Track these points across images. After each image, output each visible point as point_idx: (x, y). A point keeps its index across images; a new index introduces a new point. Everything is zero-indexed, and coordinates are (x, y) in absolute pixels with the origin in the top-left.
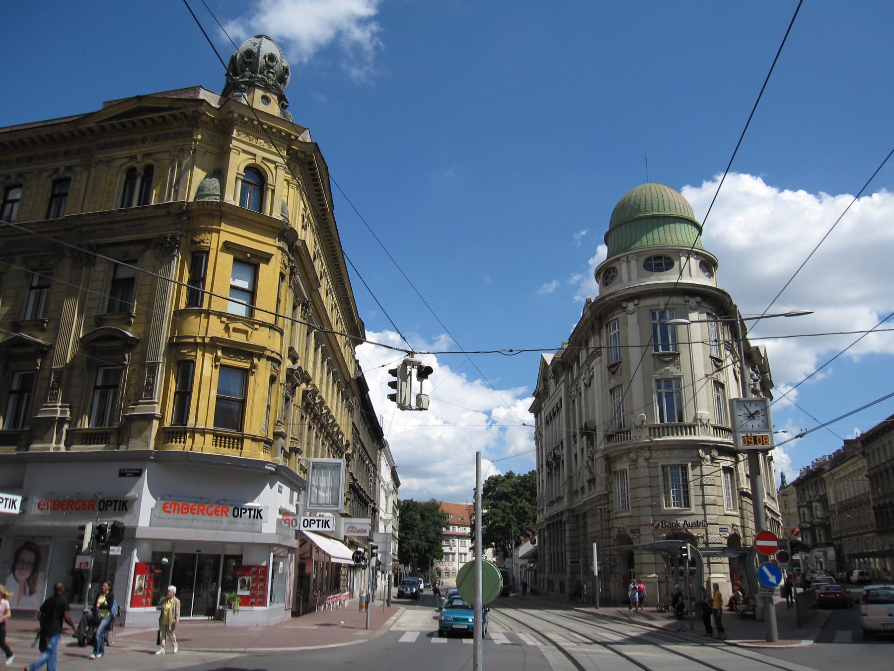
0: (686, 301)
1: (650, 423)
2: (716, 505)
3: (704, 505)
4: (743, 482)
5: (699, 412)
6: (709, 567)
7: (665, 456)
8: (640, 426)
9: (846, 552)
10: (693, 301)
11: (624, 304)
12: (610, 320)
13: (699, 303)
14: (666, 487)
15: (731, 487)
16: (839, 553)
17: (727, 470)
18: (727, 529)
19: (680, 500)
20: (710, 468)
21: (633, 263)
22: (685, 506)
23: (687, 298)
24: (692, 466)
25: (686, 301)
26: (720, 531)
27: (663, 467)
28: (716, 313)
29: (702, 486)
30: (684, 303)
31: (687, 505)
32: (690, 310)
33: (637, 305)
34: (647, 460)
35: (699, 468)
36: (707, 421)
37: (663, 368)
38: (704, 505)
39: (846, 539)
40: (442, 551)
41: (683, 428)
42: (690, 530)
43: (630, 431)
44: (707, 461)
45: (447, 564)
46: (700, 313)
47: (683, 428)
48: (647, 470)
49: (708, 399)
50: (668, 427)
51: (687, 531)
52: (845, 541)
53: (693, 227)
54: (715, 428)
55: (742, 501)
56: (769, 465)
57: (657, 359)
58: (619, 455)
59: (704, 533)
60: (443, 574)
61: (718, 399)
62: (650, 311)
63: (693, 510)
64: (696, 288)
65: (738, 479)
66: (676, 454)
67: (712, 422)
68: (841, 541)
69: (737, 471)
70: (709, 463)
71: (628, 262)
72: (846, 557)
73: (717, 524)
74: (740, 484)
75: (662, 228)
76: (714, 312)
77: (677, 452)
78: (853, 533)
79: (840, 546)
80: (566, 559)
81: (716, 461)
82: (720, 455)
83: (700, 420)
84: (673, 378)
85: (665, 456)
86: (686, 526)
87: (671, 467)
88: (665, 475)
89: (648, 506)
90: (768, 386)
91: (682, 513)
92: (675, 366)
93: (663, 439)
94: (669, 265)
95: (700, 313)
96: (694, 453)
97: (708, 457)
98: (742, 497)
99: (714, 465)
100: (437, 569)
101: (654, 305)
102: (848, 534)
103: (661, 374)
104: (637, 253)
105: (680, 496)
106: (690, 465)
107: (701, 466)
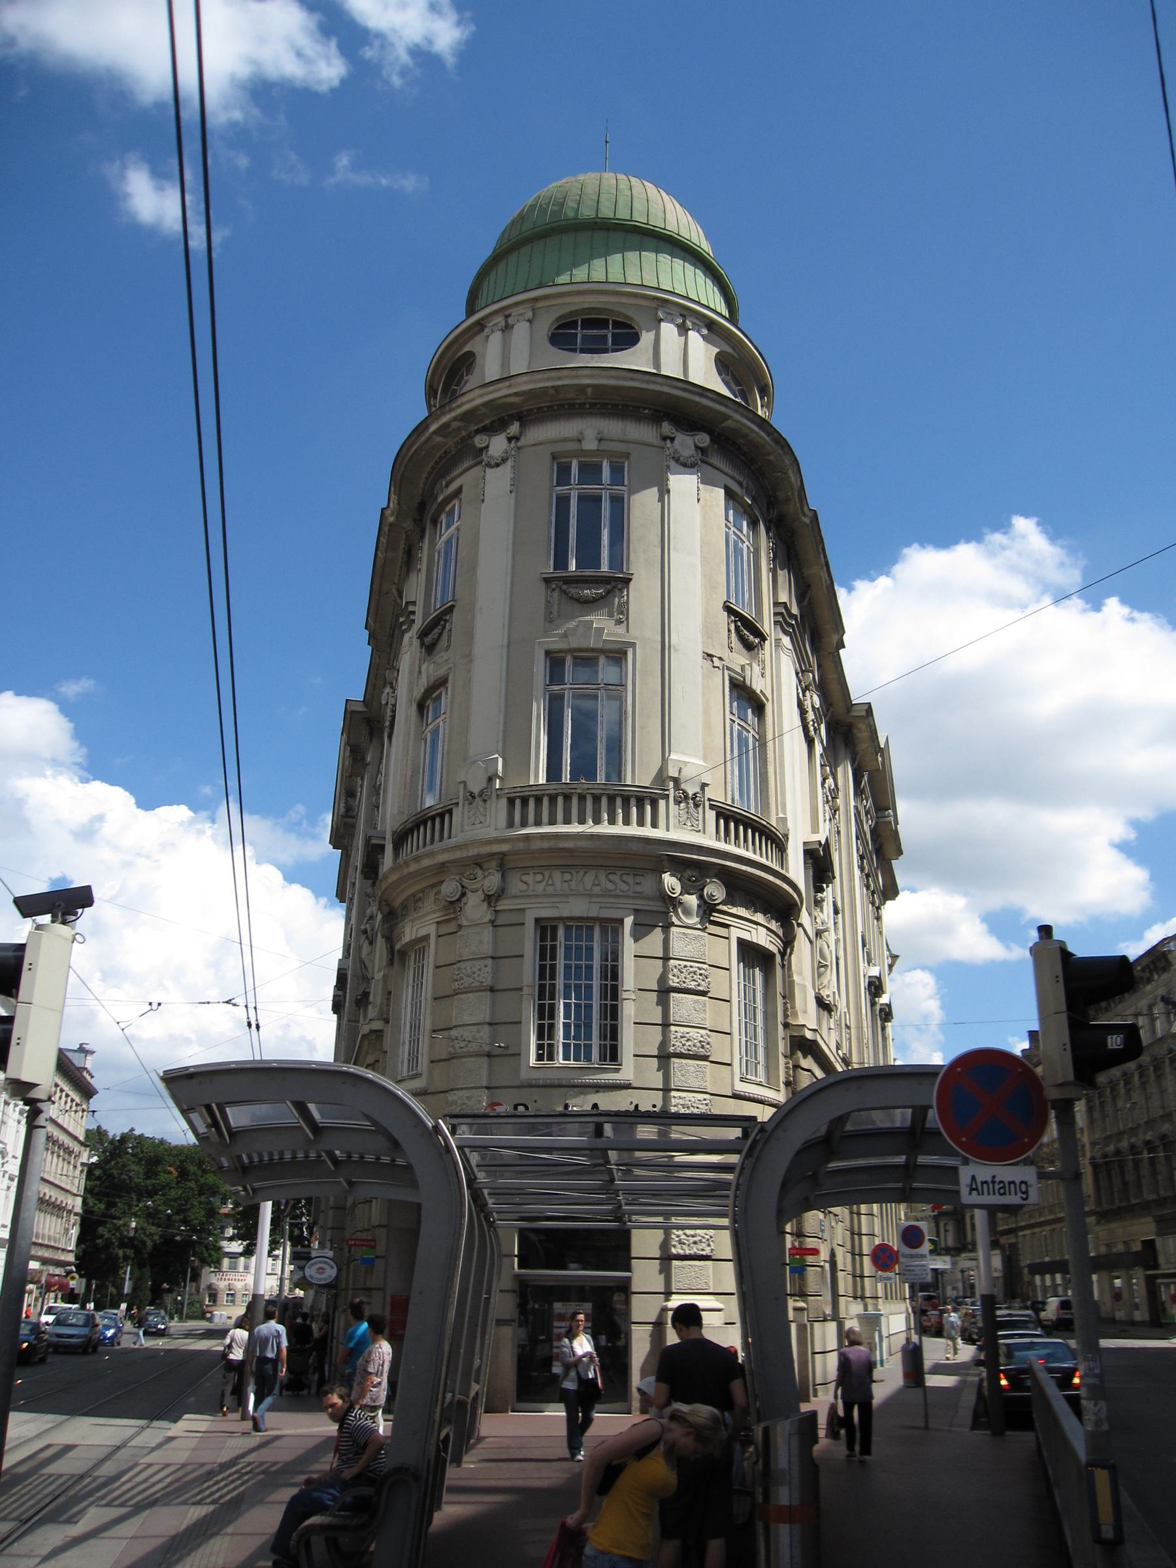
0: (665, 438)
1: (516, 782)
2: (705, 1058)
3: (665, 1057)
4: (805, 1012)
5: (673, 756)
6: (666, 1270)
8: (481, 793)
9: (1026, 1260)
10: (685, 443)
11: (479, 441)
12: (440, 499)
13: (703, 450)
14: (545, 993)
15: (765, 1013)
16: (1010, 1262)
17: (750, 954)
19: (588, 1037)
20: (696, 937)
21: (521, 331)
22: (603, 1058)
23: (667, 428)
24: (635, 924)
25: (665, 438)
27: (545, 928)
28: (753, 499)
29: (664, 992)
30: (657, 441)
31: (612, 1054)
32: (672, 464)
33: (517, 438)
34: (491, 899)
35: (658, 934)
36: (698, 789)
37: (572, 617)
38: (665, 1057)
39: (1028, 1232)
40: (220, 1248)
41: (619, 801)
43: (450, 812)
44: (687, 912)
45: (232, 1276)
47: (619, 801)
48: (487, 934)
49: (708, 726)
50: (567, 798)
52: (1024, 1236)
53: (709, 282)
54: (725, 815)
55: (797, 1067)
56: (883, 1029)
57: (556, 594)
58: (413, 895)
60: (223, 1298)
61: (743, 742)
62: (554, 457)
63: (627, 1071)
65: (789, 996)
66: (588, 885)
67: (715, 793)
68: (1017, 1236)
69: (787, 967)
70: (694, 920)
71: (507, 328)
72: (1026, 1271)
74: (795, 1014)
75: (618, 257)
76: (748, 493)
77: (589, 879)
78: (1042, 1219)
79: (1013, 1246)
81: (717, 917)
82: (730, 900)
83: (676, 781)
84: (602, 651)
85: (550, 890)
87: (568, 929)
88: (546, 953)
89: (478, 1055)
90: (889, 849)
92: (611, 615)
93: (575, 828)
94: (627, 338)
95: (705, 481)
96: (647, 885)
97: (692, 900)
98: (799, 1054)
100: (210, 1287)
101: (565, 440)
102: (1033, 1221)
103: (565, 635)
104: (536, 300)
105: (589, 1026)
106: (629, 921)
107: (667, 927)
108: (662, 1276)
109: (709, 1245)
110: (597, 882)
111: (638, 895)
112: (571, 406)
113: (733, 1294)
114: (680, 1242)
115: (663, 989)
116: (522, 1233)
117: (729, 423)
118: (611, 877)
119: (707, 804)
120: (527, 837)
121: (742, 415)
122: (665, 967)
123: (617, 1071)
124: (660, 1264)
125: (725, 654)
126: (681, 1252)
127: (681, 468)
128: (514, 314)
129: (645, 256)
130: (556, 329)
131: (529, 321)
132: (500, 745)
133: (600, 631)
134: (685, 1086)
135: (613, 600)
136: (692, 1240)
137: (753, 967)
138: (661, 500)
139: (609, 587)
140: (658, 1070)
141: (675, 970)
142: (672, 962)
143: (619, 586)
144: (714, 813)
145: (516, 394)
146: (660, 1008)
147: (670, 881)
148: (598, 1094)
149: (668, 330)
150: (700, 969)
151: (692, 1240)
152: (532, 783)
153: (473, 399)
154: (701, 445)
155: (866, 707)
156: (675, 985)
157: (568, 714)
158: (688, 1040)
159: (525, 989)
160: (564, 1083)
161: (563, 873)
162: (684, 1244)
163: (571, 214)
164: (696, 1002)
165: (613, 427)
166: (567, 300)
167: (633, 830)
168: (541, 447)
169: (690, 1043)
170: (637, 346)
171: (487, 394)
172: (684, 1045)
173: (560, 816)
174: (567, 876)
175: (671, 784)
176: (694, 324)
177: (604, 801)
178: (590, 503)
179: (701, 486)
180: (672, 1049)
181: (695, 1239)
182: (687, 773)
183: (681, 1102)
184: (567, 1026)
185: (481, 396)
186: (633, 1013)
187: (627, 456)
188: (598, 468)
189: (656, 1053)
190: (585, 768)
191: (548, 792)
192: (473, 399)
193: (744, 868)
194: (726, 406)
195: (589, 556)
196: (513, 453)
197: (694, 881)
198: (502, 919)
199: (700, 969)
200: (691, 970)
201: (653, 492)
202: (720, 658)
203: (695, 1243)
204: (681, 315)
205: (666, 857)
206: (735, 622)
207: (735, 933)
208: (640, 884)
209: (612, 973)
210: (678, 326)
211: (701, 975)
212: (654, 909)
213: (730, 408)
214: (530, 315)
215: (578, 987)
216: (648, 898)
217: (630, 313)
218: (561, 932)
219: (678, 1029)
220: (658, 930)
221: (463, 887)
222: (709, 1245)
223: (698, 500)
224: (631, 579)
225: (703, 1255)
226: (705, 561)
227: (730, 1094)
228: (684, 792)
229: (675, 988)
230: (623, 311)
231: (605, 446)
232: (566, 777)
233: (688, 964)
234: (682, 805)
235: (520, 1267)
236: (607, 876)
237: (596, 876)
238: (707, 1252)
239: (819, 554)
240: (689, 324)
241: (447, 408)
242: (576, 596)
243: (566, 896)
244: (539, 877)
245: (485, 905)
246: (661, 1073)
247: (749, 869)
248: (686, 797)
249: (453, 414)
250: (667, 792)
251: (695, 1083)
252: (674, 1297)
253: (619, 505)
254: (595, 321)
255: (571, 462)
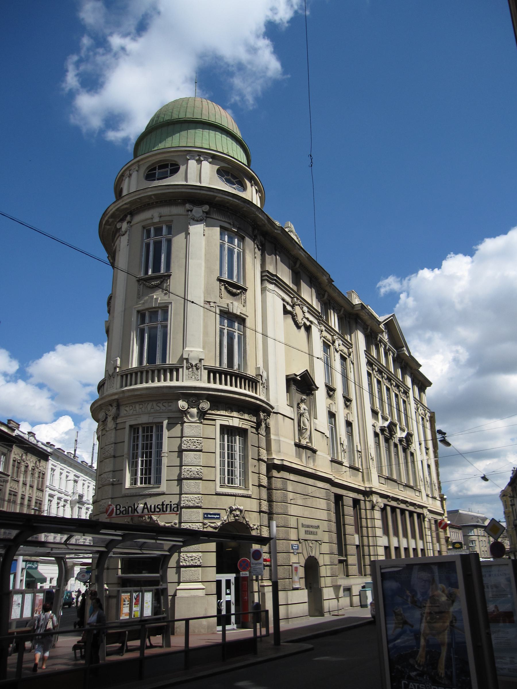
0: (188, 211)
2: (201, 479)
3: (180, 480)
6: (178, 572)
7: (135, 412)
10: (198, 211)
13: (207, 213)
18: (219, 514)
21: (134, 175)
23: (188, 206)
24: (168, 424)
25: (188, 211)
26: (205, 518)
31: (158, 481)
32: (192, 221)
33: (130, 222)
35: (179, 426)
37: (147, 295)
38: (180, 480)
41: (162, 371)
42: (154, 517)
44: (192, 416)
46: (207, 226)
47: (162, 371)
49: (206, 334)
51: (151, 518)
57: (142, 286)
59: (177, 521)
63: (163, 487)
64: (199, 191)
71: (130, 176)
73: (200, 507)
76: (234, 226)
77: (149, 407)
80: (365, 565)
81: (207, 416)
83: (187, 360)
84: (159, 307)
85: (135, 412)
86: (146, 510)
91: (147, 492)
93: (139, 386)
94: (175, 170)
97: (194, 411)
99: (206, 422)
103: (144, 303)
104: (138, 161)
106: (165, 422)
108: (177, 575)
109: (199, 561)
110: (152, 407)
111: (171, 411)
112: (149, 204)
113: (303, 578)
114: (185, 560)
115: (180, 451)
116: (123, 560)
117: (217, 198)
118: (159, 404)
119: (202, 367)
120: (133, 390)
121: (222, 194)
122: (181, 440)
123: (159, 487)
124: (176, 570)
125: (218, 300)
126: (185, 564)
127: (197, 223)
128: (132, 169)
129: (190, 132)
130: (148, 172)
131: (137, 171)
132: (120, 354)
133: (157, 299)
134: (189, 492)
135: (164, 285)
136: (190, 559)
137: (235, 436)
138: (186, 238)
139: (162, 280)
140: (177, 486)
141: (185, 442)
142: (184, 438)
143: (166, 279)
144: (206, 371)
145: (125, 204)
146: (179, 459)
147: (182, 404)
148: (151, 498)
149: (192, 163)
150: (198, 440)
151: (190, 559)
152: (130, 368)
153: (112, 209)
154: (205, 211)
155: (360, 305)
156: (185, 448)
157: (146, 336)
158: (191, 472)
159: (125, 455)
160: (137, 494)
161: (139, 405)
162: (187, 561)
163: (162, 120)
164: (195, 455)
165: (166, 210)
166: (150, 159)
167: (168, 383)
168: (139, 224)
169: (191, 473)
170: (178, 173)
171: (116, 206)
172: (188, 474)
173: (139, 381)
174: (141, 406)
175: (185, 361)
176: (204, 158)
177: (156, 372)
178: (158, 245)
179: (206, 228)
180: (182, 477)
181: (192, 558)
182: (192, 355)
183: (186, 499)
184: (142, 470)
185: (114, 207)
186: (166, 462)
187: (172, 221)
188: (161, 229)
189: (176, 478)
190: (152, 359)
191: (134, 371)
192: (112, 209)
193: (220, 394)
194: (213, 192)
195: (156, 268)
196: (129, 228)
197: (194, 402)
198: (119, 427)
199: (198, 440)
200: (193, 441)
201: (183, 234)
202: (215, 302)
203: (192, 560)
204: (198, 155)
205: (180, 394)
206: (225, 285)
207: (218, 423)
208: (171, 406)
209: (160, 445)
210: (197, 161)
211: (198, 443)
212: (177, 416)
213: (215, 192)
214: (137, 168)
215: (146, 453)
216: (174, 412)
217: (176, 159)
218: (140, 430)
219: (185, 467)
220: (179, 425)
221: (107, 415)
222: (199, 561)
223: (204, 235)
224: (171, 275)
225: (195, 565)
226: (207, 260)
227: (215, 494)
228: (191, 364)
229: (185, 449)
230: (172, 159)
231: (163, 219)
232: (145, 363)
233: (191, 438)
234: (190, 370)
235: (122, 573)
236: (157, 405)
237: (152, 405)
238: (198, 563)
239: (294, 244)
240: (202, 158)
241: (105, 214)
242: (149, 286)
243: (140, 414)
244: (131, 407)
245: (113, 421)
246: (178, 487)
247: (223, 394)
248: (192, 366)
249: (108, 216)
250: (183, 365)
251: (194, 490)
252: (181, 584)
253: (169, 242)
254: (163, 165)
255: (151, 228)
